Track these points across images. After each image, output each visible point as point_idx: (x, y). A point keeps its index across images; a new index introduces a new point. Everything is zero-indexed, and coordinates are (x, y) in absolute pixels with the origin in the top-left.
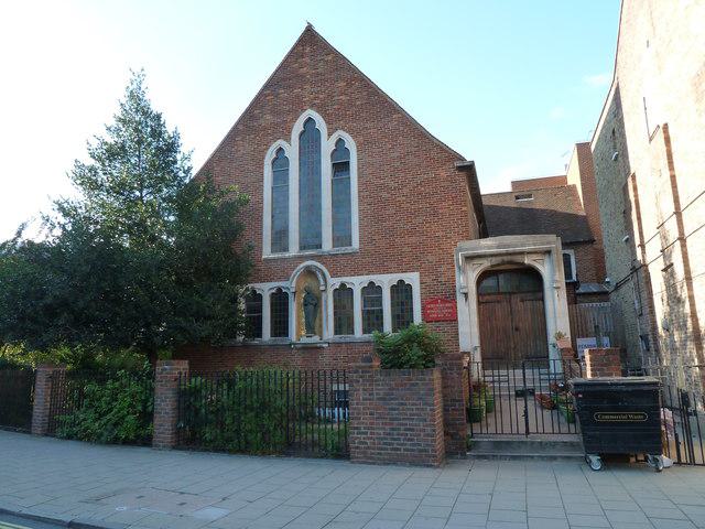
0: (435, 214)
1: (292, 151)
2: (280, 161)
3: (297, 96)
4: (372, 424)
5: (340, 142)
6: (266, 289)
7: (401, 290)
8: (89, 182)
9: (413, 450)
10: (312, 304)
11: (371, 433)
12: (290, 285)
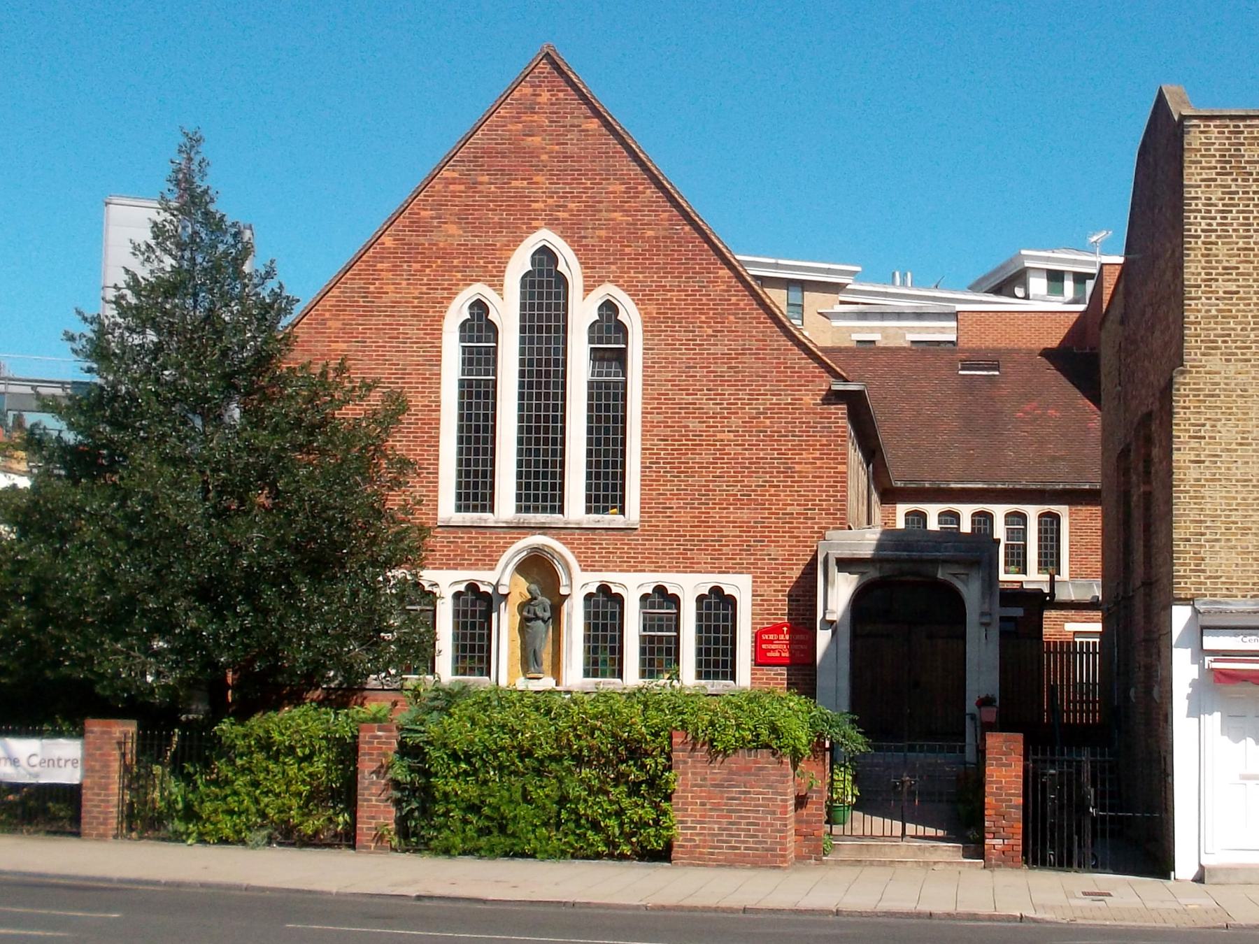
0: (787, 472)
1: (507, 314)
2: (480, 325)
3: (520, 196)
4: (703, 816)
5: (609, 308)
6: (445, 582)
7: (717, 607)
8: (99, 352)
9: (757, 849)
10: (543, 610)
11: (702, 828)
12: (501, 575)
